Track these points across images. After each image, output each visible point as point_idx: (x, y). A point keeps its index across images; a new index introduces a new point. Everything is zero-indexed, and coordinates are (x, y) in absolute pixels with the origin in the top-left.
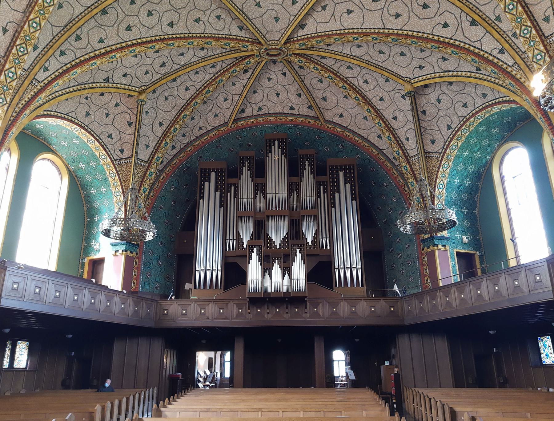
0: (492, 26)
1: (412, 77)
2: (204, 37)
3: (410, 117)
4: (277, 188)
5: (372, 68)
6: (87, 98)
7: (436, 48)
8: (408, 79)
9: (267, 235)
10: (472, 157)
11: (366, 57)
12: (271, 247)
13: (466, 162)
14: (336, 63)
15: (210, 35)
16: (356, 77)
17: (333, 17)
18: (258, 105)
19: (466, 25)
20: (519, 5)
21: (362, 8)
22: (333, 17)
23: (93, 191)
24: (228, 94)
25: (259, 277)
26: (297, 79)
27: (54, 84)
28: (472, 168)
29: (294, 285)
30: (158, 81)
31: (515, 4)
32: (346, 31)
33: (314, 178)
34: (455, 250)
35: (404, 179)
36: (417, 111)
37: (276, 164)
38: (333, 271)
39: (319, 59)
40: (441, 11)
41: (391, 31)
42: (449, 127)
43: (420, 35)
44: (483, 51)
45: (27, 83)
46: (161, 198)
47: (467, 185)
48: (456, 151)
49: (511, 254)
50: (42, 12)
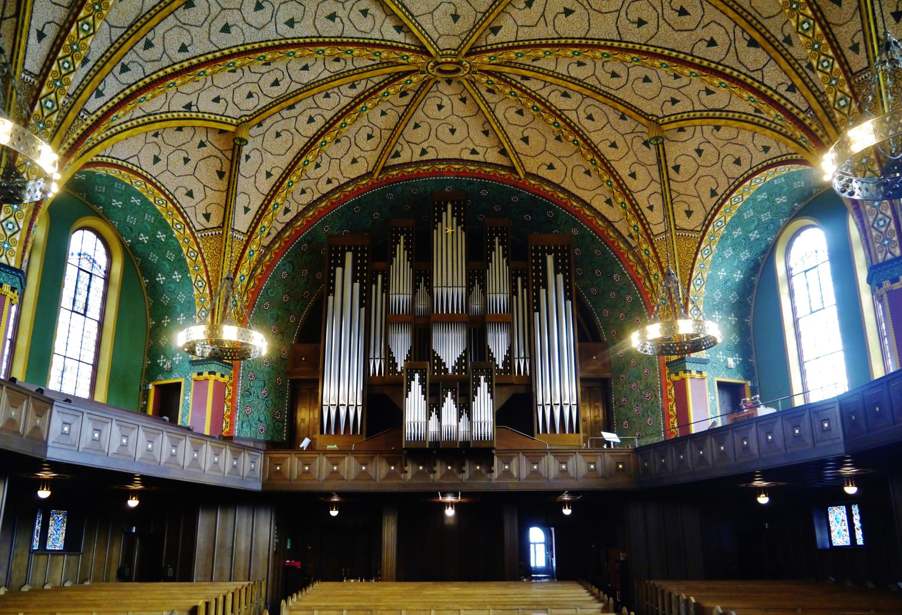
0: (778, 48)
1: (661, 115)
2: (342, 44)
3: (655, 174)
4: (450, 284)
5: (600, 98)
6: (156, 135)
7: (696, 76)
10: (746, 238)
11: (591, 81)
12: (439, 371)
13: (736, 245)
14: (544, 86)
15: (350, 40)
16: (576, 110)
17: (542, 19)
19: (742, 45)
20: (817, 24)
21: (588, 7)
22: (542, 19)
23: (161, 279)
24: (375, 128)
25: (422, 418)
26: (483, 108)
27: (111, 117)
28: (745, 255)
29: (475, 431)
30: (266, 108)
31: (812, 22)
32: (563, 41)
33: (508, 264)
34: (716, 379)
35: (644, 268)
36: (666, 167)
37: (449, 240)
38: (534, 408)
39: (519, 79)
40: (706, 21)
41: (630, 46)
42: (713, 193)
43: (674, 54)
44: (765, 85)
45: (71, 116)
46: (267, 290)
47: (737, 280)
48: (722, 229)
49: (796, 387)
50: (97, 7)
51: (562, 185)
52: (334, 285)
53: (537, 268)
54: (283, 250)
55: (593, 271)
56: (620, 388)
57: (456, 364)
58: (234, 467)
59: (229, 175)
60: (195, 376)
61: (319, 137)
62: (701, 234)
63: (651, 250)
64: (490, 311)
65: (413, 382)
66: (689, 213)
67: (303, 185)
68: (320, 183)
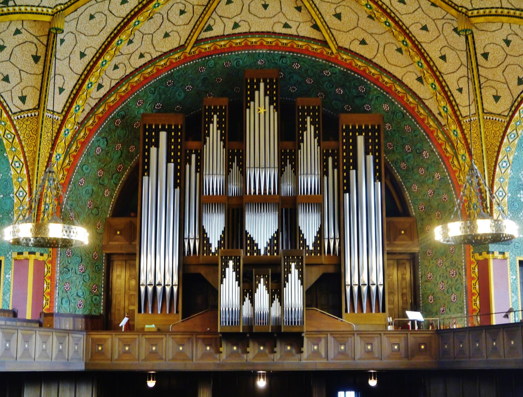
1: (470, 8)
3: (464, 59)
8: (464, 10)
9: (247, 233)
18: (233, 20)
24: (187, 4)
33: (319, 145)
34: (518, 259)
35: (453, 147)
37: (261, 117)
51: (374, 61)
52: (148, 164)
53: (348, 147)
54: (97, 126)
55: (403, 146)
56: (426, 263)
57: (268, 245)
58: (60, 351)
59: (45, 58)
60: (15, 255)
61: (133, 17)
62: (508, 119)
63: (459, 132)
64: (301, 192)
65: (227, 269)
66: (497, 98)
67: (116, 61)
68: (132, 58)
